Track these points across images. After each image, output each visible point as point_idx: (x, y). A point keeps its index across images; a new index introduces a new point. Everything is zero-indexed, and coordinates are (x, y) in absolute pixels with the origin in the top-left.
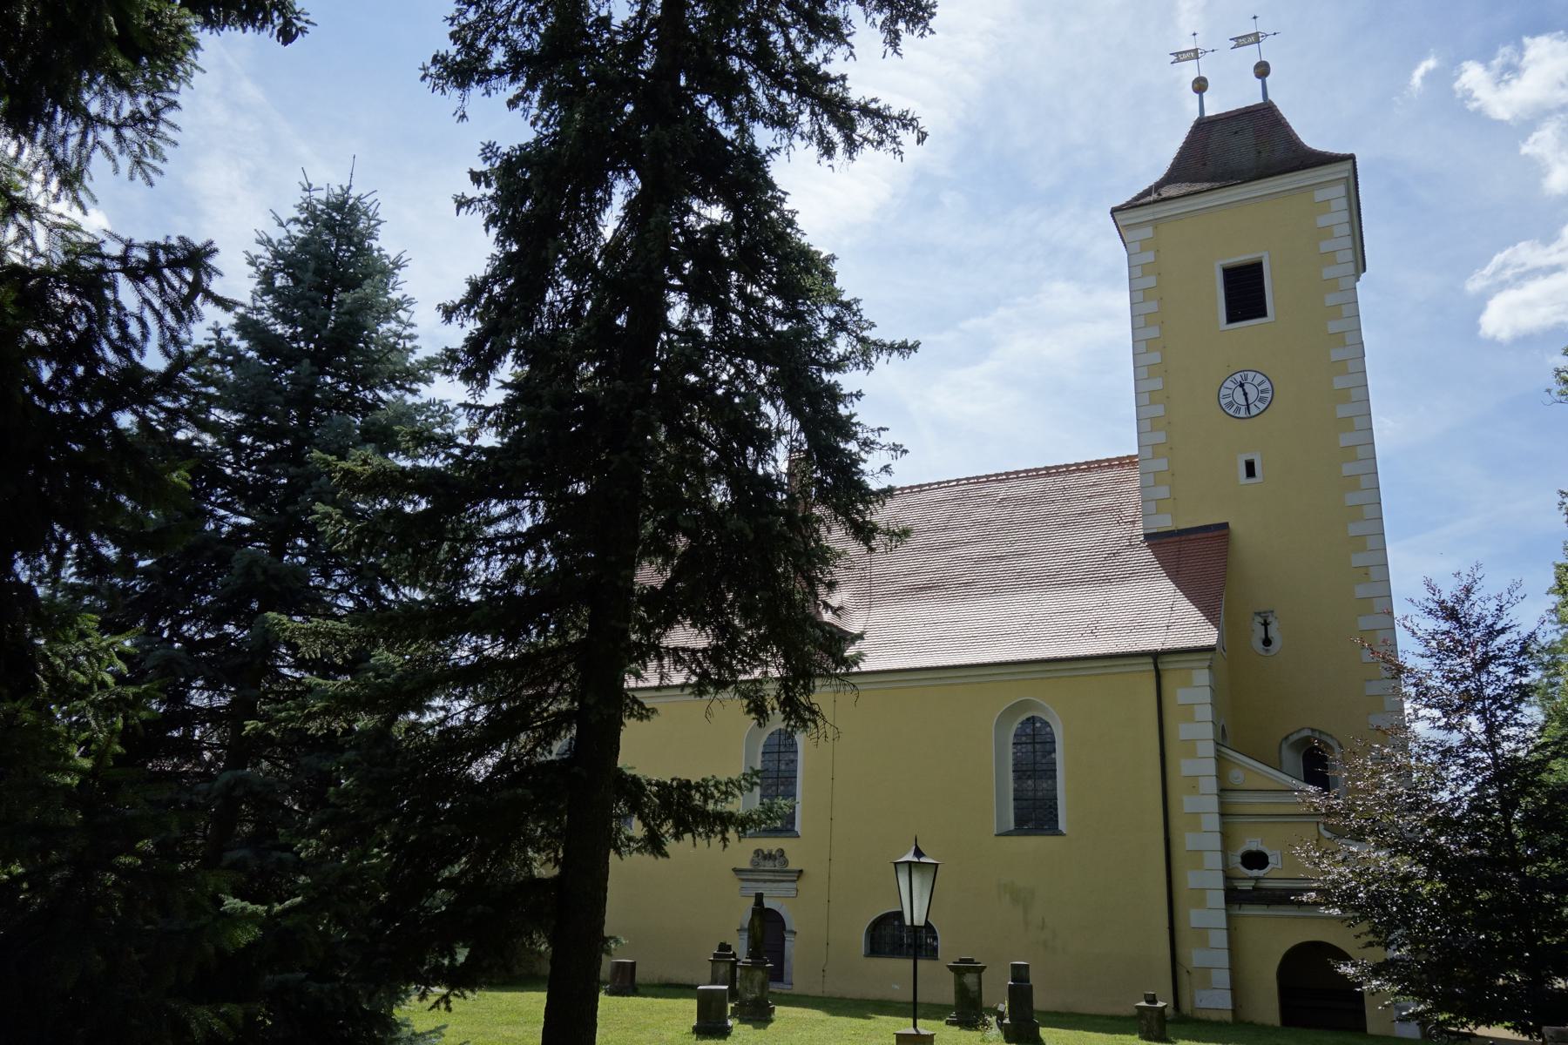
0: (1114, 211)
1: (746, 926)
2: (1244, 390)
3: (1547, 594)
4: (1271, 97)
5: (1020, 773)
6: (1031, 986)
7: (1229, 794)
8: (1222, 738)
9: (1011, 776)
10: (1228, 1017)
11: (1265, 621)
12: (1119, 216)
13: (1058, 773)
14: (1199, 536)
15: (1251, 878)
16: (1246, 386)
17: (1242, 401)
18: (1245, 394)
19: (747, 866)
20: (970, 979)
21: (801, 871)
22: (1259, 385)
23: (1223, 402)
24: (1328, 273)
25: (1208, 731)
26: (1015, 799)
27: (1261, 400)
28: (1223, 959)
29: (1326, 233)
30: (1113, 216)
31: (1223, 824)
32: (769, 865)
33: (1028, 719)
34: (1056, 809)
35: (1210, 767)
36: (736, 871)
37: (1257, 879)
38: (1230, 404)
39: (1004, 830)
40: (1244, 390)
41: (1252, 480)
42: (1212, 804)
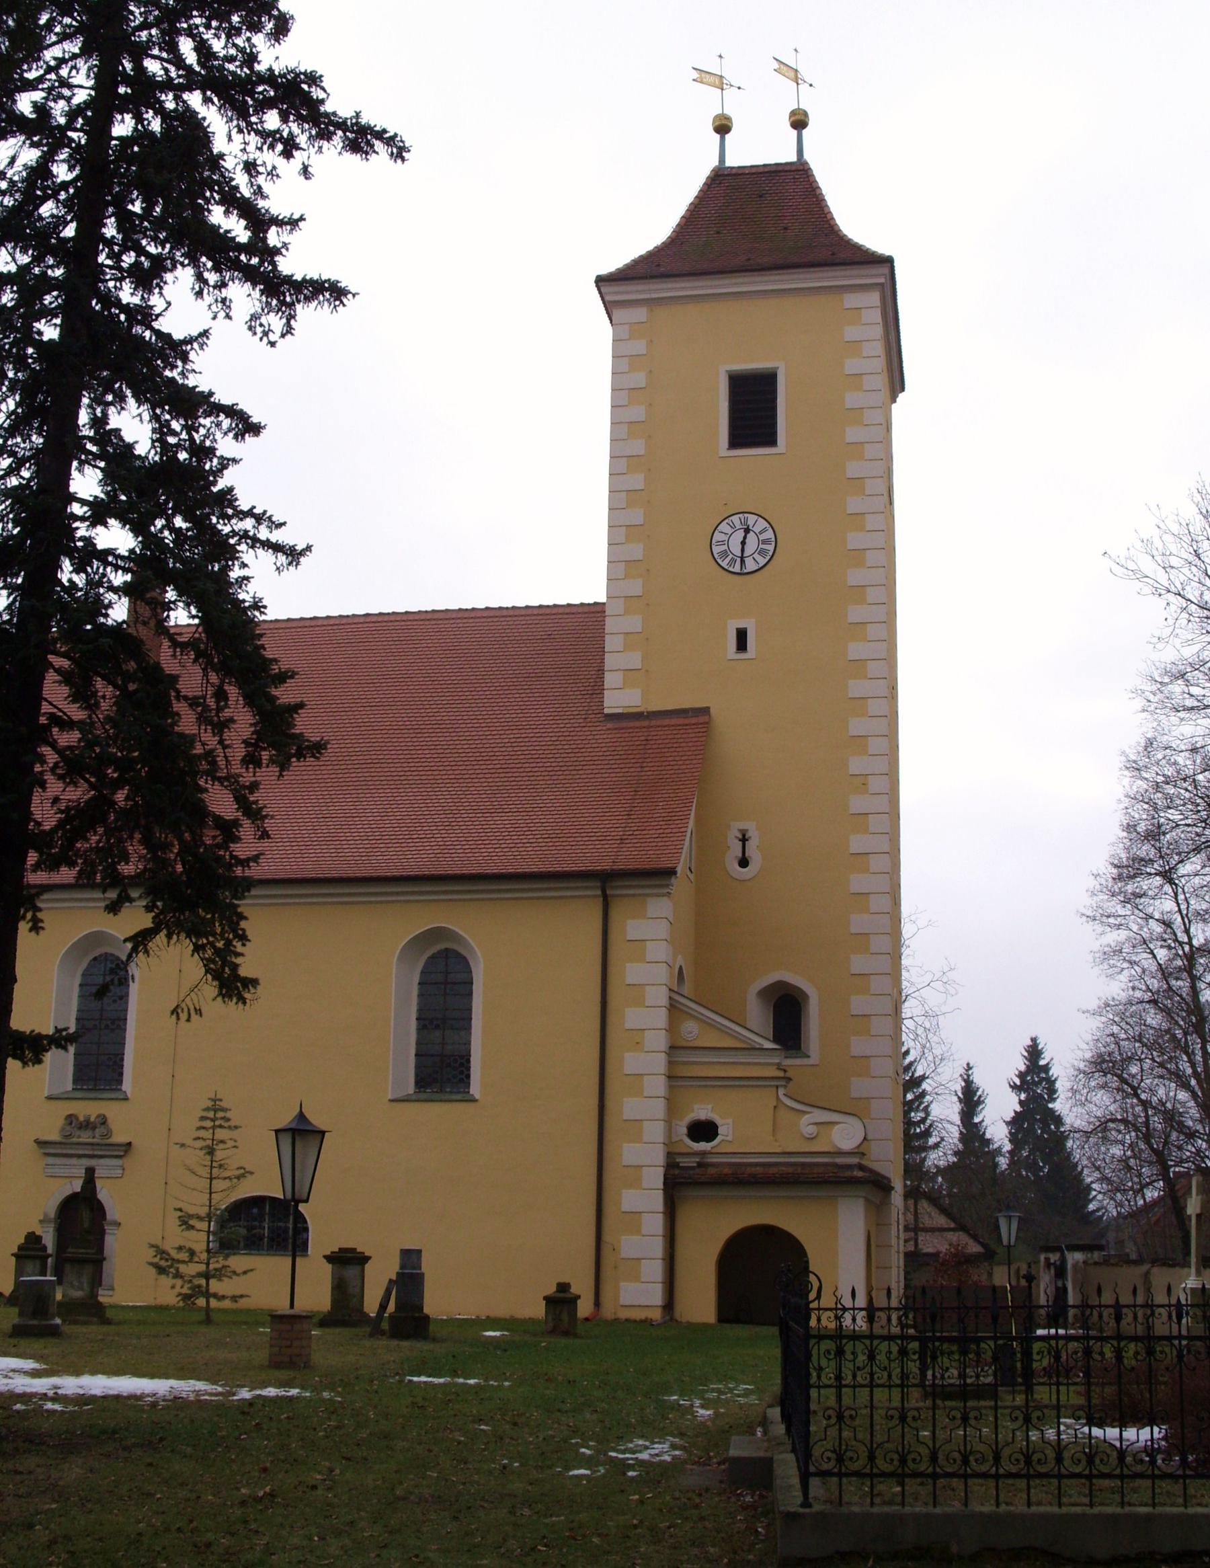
0: (600, 281)
1: (52, 1214)
2: (745, 538)
3: (241, 460)
4: (807, 156)
5: (426, 1022)
6: (423, 1274)
9: (413, 1025)
10: (656, 1315)
11: (744, 836)
14: (674, 721)
15: (696, 1154)
16: (751, 536)
17: (737, 550)
18: (743, 543)
19: (54, 1136)
20: (351, 1272)
21: (129, 1144)
22: (761, 533)
23: (716, 550)
24: (853, 399)
25: (661, 974)
27: (762, 552)
29: (855, 347)
30: (597, 286)
32: (85, 1137)
33: (439, 952)
34: (469, 1069)
35: (660, 1018)
36: (41, 1143)
37: (703, 1154)
38: (724, 554)
39: (400, 1095)
40: (745, 538)
42: (659, 1063)
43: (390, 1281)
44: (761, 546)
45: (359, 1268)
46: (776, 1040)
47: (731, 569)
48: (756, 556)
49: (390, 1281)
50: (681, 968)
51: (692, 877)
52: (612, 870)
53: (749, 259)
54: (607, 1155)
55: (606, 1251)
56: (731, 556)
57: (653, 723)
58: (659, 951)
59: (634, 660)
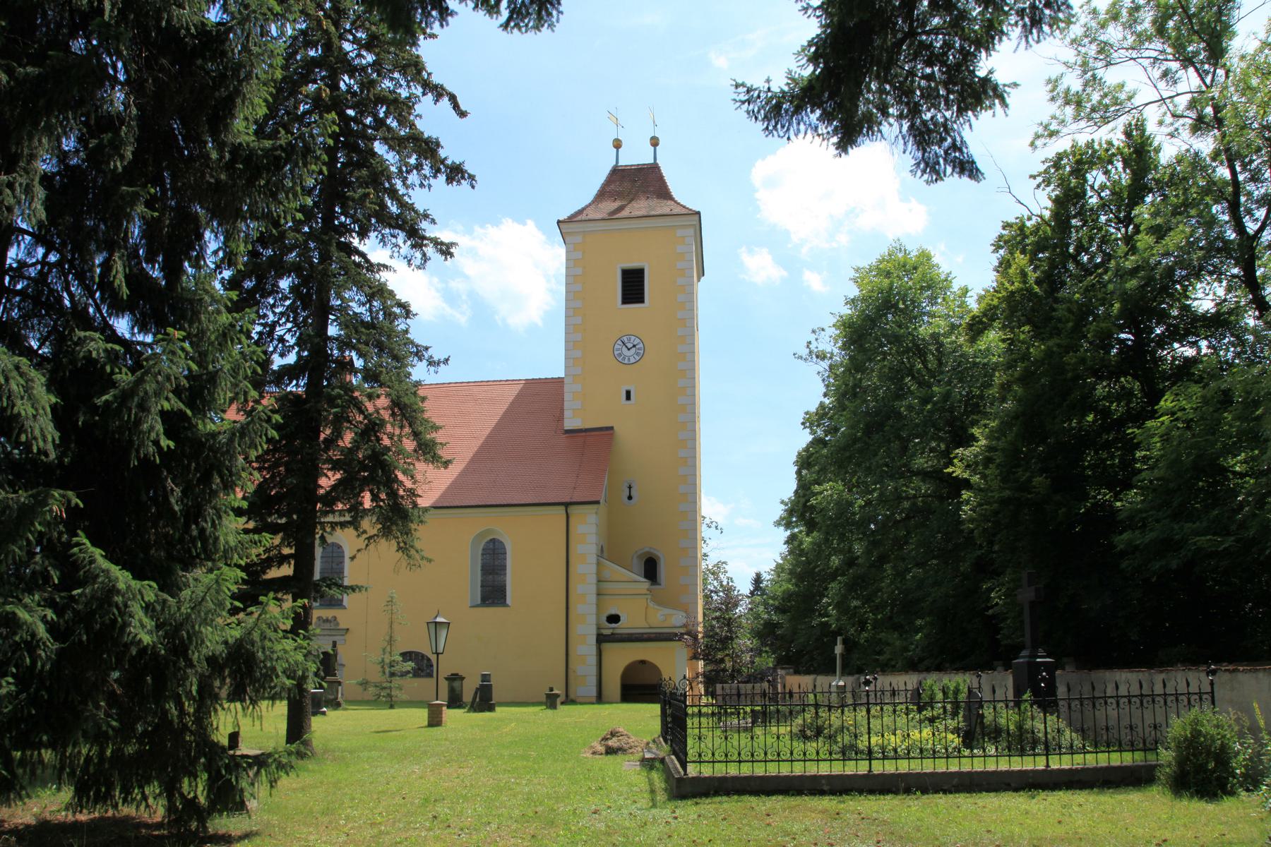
8: (601, 553)
12: (562, 225)
20: (456, 684)
23: (616, 353)
27: (620, 355)
28: (593, 670)
31: (598, 600)
32: (327, 626)
35: (593, 569)
38: (638, 354)
41: (628, 402)
42: (593, 589)
46: (646, 577)
54: (571, 652)
55: (570, 671)
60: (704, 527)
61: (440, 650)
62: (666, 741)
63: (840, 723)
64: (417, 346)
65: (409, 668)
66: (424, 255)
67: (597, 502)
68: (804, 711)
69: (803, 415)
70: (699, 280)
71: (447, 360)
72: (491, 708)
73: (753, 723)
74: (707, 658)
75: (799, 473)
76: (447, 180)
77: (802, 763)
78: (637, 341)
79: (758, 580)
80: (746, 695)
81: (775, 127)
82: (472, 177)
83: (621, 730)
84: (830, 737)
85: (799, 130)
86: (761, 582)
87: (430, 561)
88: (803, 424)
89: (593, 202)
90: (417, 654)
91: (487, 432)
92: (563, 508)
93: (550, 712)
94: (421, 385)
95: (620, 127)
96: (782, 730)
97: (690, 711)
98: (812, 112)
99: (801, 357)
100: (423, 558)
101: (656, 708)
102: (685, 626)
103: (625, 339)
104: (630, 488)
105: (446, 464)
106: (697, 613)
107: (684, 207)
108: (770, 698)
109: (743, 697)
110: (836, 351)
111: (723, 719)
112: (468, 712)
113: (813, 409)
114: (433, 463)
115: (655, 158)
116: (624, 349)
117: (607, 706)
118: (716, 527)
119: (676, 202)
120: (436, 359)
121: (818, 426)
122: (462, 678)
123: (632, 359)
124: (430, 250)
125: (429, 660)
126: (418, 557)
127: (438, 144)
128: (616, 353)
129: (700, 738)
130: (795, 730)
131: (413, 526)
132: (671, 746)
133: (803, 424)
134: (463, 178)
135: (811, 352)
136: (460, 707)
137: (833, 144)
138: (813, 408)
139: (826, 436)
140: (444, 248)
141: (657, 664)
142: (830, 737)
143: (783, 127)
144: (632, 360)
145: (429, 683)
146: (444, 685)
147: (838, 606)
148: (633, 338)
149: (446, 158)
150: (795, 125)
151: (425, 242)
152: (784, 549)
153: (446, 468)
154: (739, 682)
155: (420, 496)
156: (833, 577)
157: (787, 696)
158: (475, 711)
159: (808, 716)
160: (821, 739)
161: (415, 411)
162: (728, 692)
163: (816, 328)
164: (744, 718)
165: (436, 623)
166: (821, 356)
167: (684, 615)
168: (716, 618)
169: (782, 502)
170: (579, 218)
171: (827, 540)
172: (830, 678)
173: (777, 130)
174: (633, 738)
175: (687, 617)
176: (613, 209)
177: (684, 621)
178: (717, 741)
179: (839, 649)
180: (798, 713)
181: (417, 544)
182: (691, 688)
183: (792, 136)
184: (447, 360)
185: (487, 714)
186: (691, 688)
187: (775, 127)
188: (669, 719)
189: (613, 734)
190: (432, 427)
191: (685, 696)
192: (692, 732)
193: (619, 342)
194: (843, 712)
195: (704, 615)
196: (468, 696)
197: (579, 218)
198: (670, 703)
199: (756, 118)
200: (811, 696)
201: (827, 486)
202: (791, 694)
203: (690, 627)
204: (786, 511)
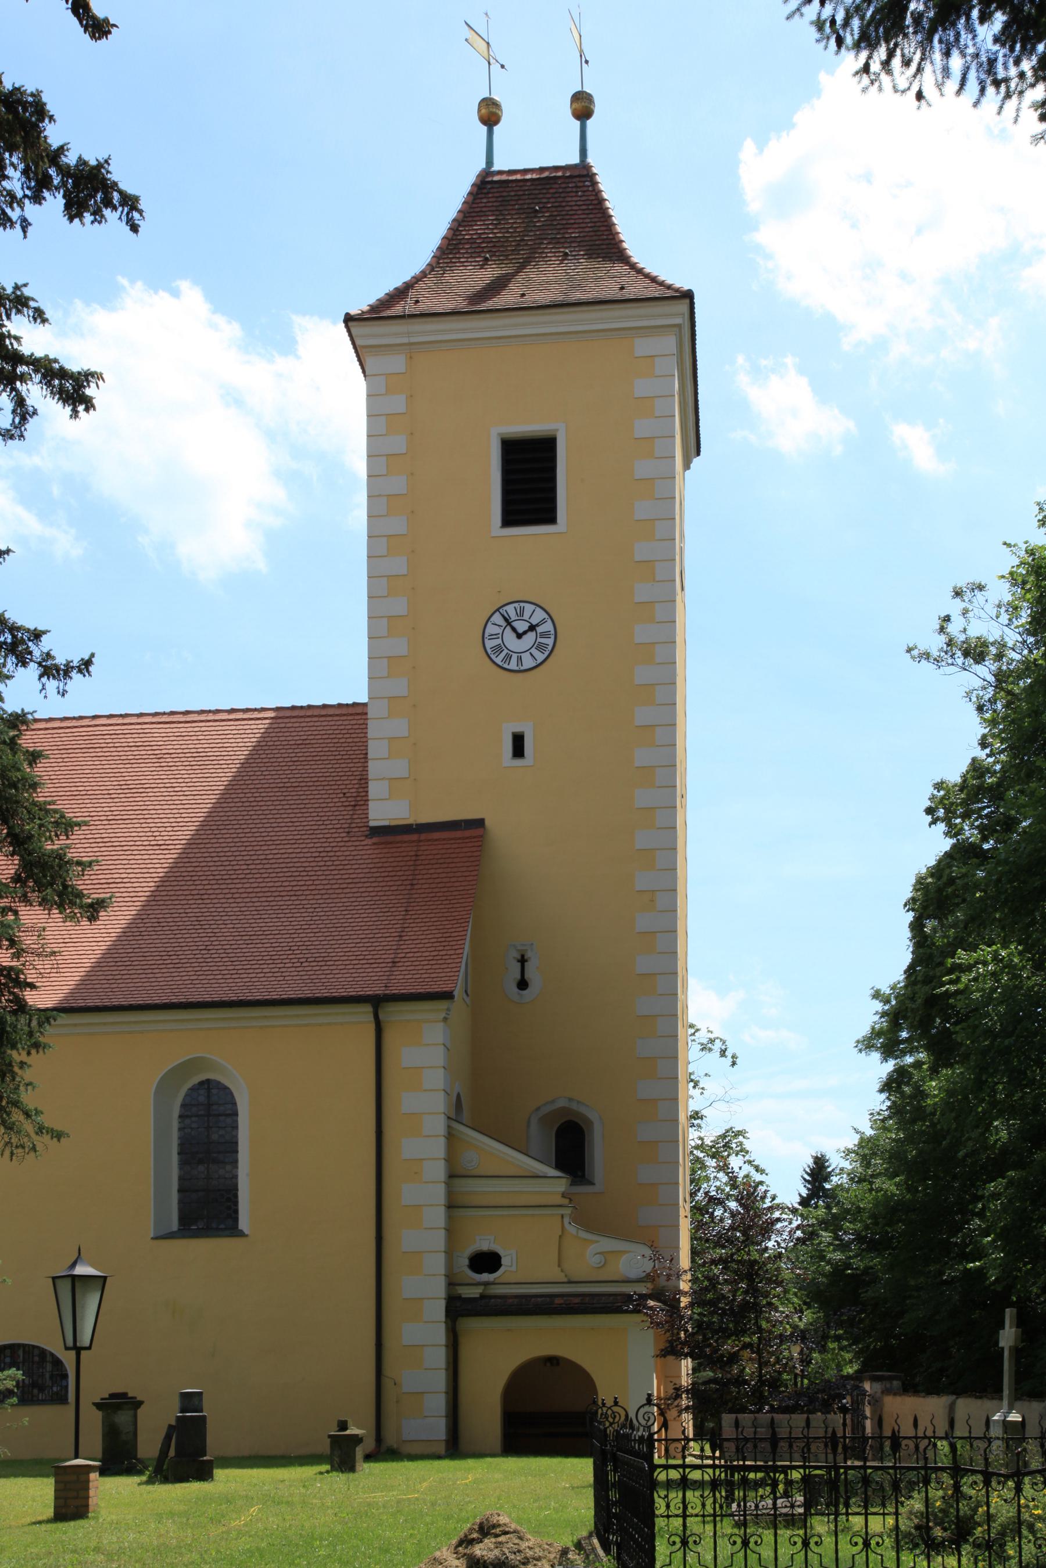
4: (590, 160)
7: (463, 1181)
8: (457, 1111)
9: (175, 1158)
11: (523, 956)
12: (357, 329)
13: (240, 1194)
15: (478, 1284)
20: (122, 1418)
23: (489, 644)
26: (179, 1191)
27: (498, 649)
28: (439, 1381)
30: (347, 327)
31: (450, 1219)
33: (202, 1083)
34: (236, 1203)
35: (438, 1148)
37: (486, 1284)
38: (540, 647)
41: (519, 762)
42: (439, 1194)
43: (170, 1426)
44: (506, 651)
45: (132, 1412)
46: (559, 1166)
47: (506, 666)
48: (534, 651)
49: (170, 1426)
50: (458, 1095)
51: (468, 1000)
52: (385, 995)
53: (523, 295)
55: (387, 1384)
56: (506, 651)
57: (423, 836)
58: (436, 1079)
59: (399, 768)
60: (694, 1052)
61: (85, 1339)
62: (606, 1546)
63: (1012, 1512)
64: (13, 629)
65: (10, 1384)
66: (20, 402)
67: (448, 996)
68: (927, 1482)
69: (930, 790)
70: (687, 466)
71: (86, 665)
72: (204, 1473)
73: (808, 1505)
74: (703, 1358)
75: (916, 927)
76: (68, 207)
77: (882, 1517)
78: (539, 616)
79: (819, 1171)
80: (791, 1440)
81: (886, 64)
82: (130, 202)
83: (503, 1519)
84: (988, 1545)
85: (946, 71)
86: (827, 1178)
87: (58, 1135)
88: (929, 811)
89: (431, 267)
90: (29, 1350)
91: (186, 833)
92: (365, 1012)
93: (339, 1479)
94: (25, 722)
95: (495, 67)
96: (876, 1524)
97: (661, 1476)
98: (984, 18)
99: (926, 656)
100: (40, 1130)
101: (583, 1469)
102: (649, 1278)
103: (511, 610)
104: (523, 961)
105: (94, 910)
106: (677, 1248)
107: (654, 280)
108: (845, 1448)
109: (783, 1445)
110: (1012, 637)
111: (738, 1494)
112: (150, 1481)
113: (954, 776)
114: (61, 906)
115: (583, 152)
116: (509, 635)
117: (470, 1462)
118: (723, 1053)
119: (633, 266)
120: (60, 660)
121: (965, 816)
122: (137, 1404)
123: (526, 657)
124: (35, 392)
125: (57, 1363)
126: (28, 1127)
127: (40, 110)
128: (489, 644)
129: (685, 1543)
130: (905, 1525)
131: (16, 1056)
132: (618, 1558)
133: (929, 811)
134: (108, 203)
135: (950, 643)
136: (130, 1471)
137: (1036, 106)
138: (954, 773)
139: (985, 839)
140: (68, 385)
141: (579, 1361)
142: (988, 1545)
143: (907, 63)
144: (528, 662)
145: (60, 1416)
146: (93, 1422)
147: (1005, 1236)
148: (529, 608)
149: (61, 149)
150: (937, 56)
151: (21, 369)
152: (880, 1102)
153: (93, 918)
154: (772, 1410)
155: (32, 986)
156: (996, 1168)
157: (887, 1444)
158: (166, 1480)
159: (936, 1494)
160: (966, 1549)
161: (14, 785)
162: (749, 1433)
163: (961, 583)
164: (786, 1495)
165: (74, 1278)
166: (975, 652)
167: (648, 1252)
168: (721, 1260)
169: (877, 995)
170: (397, 309)
171: (979, 1085)
172: (988, 1404)
173: (889, 72)
174: (532, 1540)
175: (656, 1257)
176: (480, 285)
177: (648, 1267)
178: (725, 1549)
179: (1008, 1337)
180: (912, 1486)
181: (27, 1098)
182: (665, 1425)
183: (930, 91)
184: (86, 665)
185: (194, 1487)
186: (665, 1425)
187: (886, 64)
188: (613, 1495)
189: (486, 1530)
190: (57, 824)
191: (650, 1441)
192: (667, 1527)
193: (497, 618)
194: (1018, 1490)
195: (694, 1253)
196: (148, 1445)
197: (397, 309)
198: (615, 1459)
199: (840, 41)
200: (943, 1446)
201: (985, 951)
202: (896, 1441)
203: (662, 1282)
204: (884, 1014)
